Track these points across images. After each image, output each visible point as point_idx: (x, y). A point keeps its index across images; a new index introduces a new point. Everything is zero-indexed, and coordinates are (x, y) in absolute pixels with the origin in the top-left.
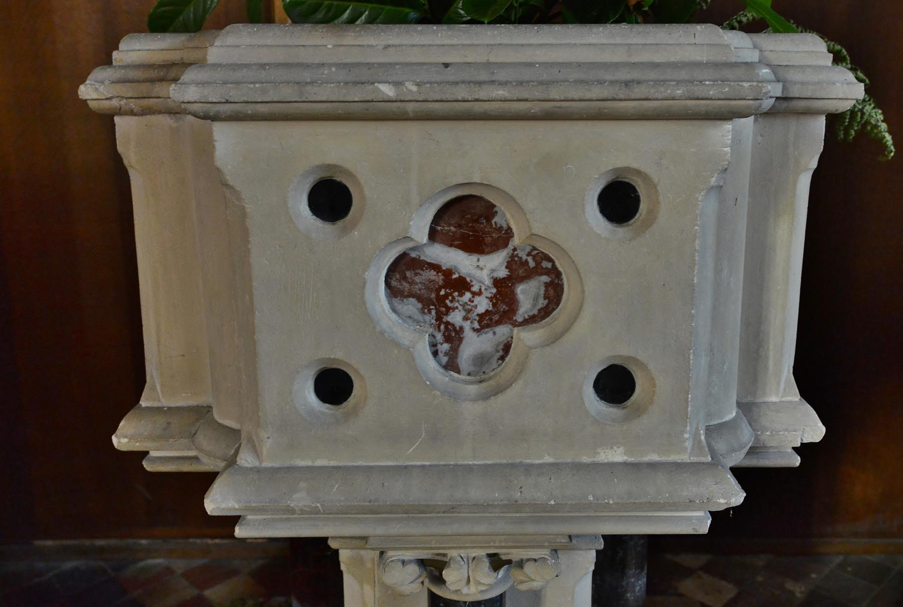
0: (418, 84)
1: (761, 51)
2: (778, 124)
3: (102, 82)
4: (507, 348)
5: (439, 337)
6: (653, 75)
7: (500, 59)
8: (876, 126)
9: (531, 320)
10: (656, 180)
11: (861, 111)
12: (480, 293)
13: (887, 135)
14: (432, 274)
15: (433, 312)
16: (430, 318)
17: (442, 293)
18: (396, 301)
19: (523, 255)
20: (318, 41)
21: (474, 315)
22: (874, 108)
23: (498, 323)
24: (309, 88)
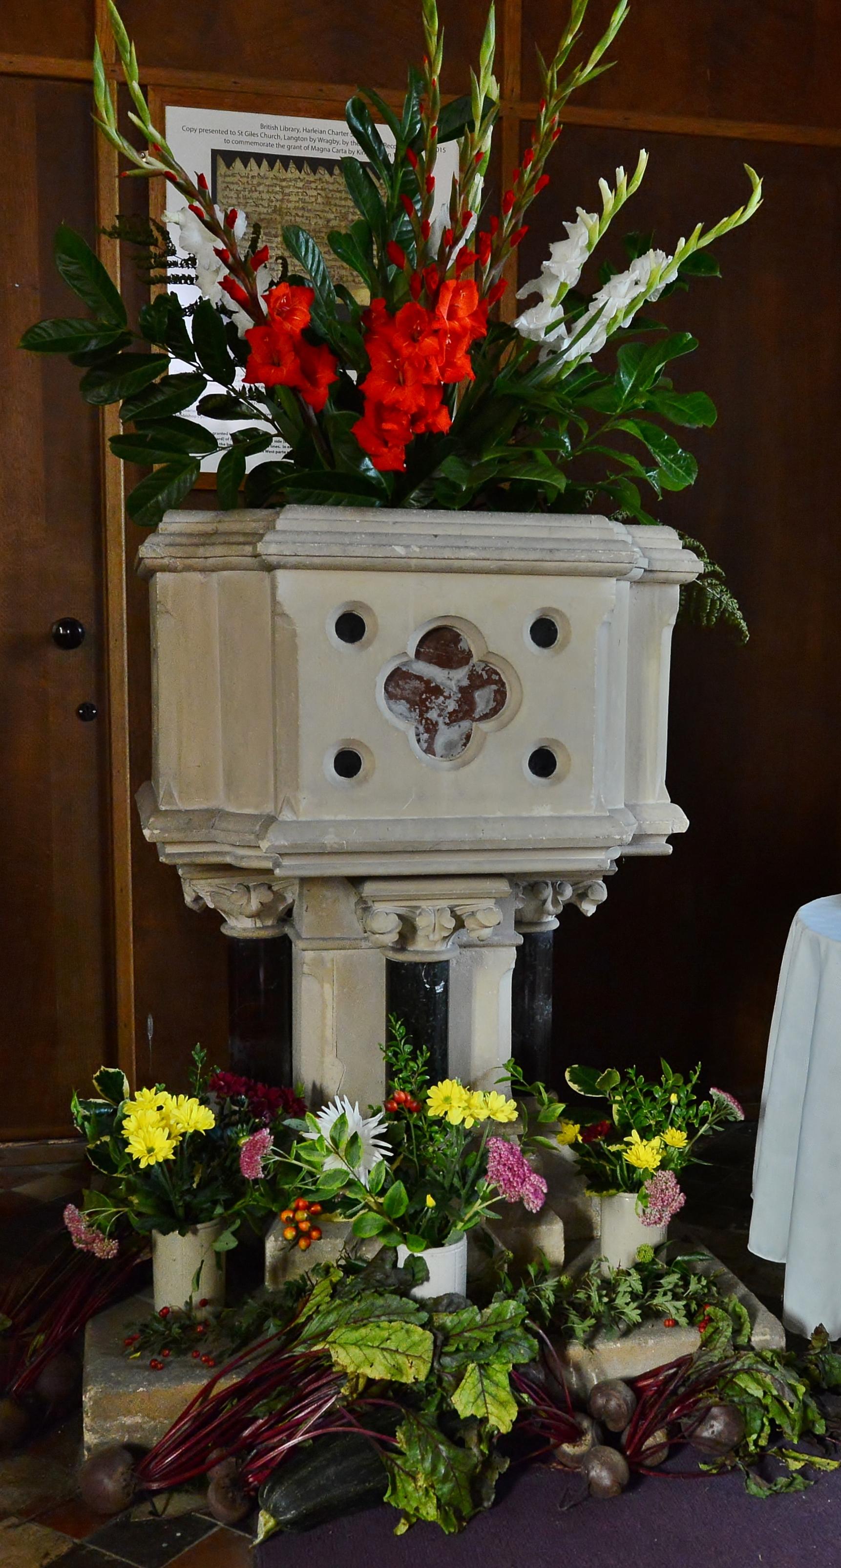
0: (420, 547)
1: (633, 537)
2: (646, 590)
3: (158, 545)
4: (468, 737)
5: (421, 729)
6: (565, 546)
7: (469, 534)
8: (733, 614)
9: (485, 717)
10: (568, 615)
11: (720, 599)
12: (449, 697)
13: (742, 621)
14: (417, 683)
15: (417, 711)
16: (415, 715)
17: (424, 696)
18: (391, 702)
19: (479, 670)
20: (353, 518)
21: (445, 713)
22: (731, 598)
23: (462, 719)
24: (350, 547)
